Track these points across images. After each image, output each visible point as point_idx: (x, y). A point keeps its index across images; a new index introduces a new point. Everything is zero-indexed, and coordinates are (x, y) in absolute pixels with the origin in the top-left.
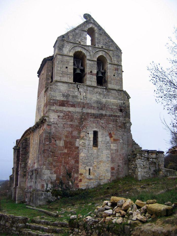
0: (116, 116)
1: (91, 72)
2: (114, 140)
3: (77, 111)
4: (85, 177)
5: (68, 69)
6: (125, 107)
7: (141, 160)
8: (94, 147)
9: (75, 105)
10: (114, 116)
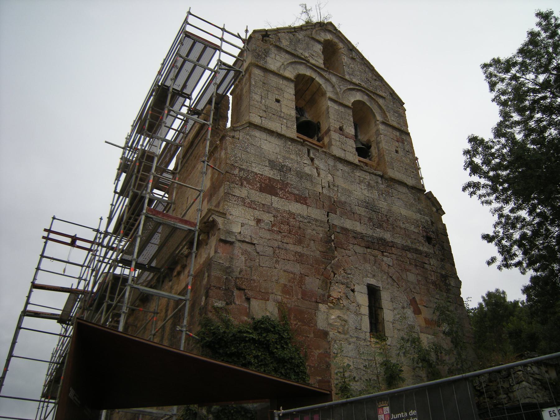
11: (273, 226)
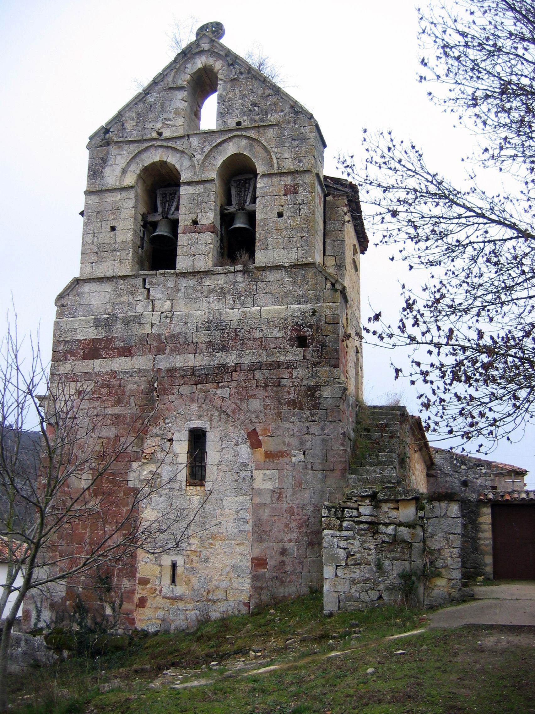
0: (279, 365)
1: (195, 222)
2: (269, 455)
3: (137, 367)
4: (157, 592)
5: (115, 234)
6: (318, 328)
7: (338, 533)
8: (191, 488)
9: (131, 347)
10: (271, 364)
11: (93, 393)
